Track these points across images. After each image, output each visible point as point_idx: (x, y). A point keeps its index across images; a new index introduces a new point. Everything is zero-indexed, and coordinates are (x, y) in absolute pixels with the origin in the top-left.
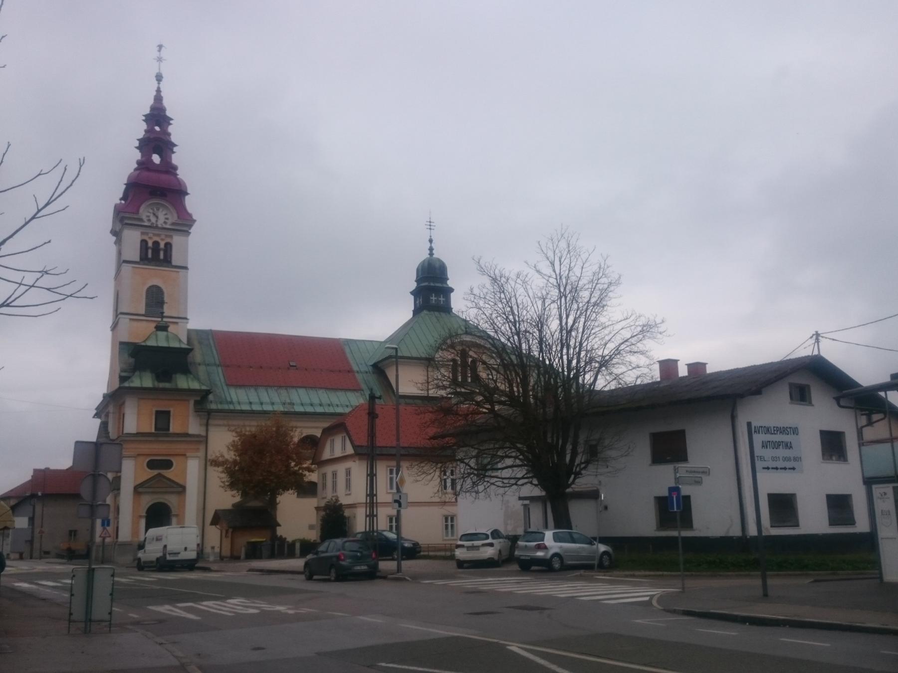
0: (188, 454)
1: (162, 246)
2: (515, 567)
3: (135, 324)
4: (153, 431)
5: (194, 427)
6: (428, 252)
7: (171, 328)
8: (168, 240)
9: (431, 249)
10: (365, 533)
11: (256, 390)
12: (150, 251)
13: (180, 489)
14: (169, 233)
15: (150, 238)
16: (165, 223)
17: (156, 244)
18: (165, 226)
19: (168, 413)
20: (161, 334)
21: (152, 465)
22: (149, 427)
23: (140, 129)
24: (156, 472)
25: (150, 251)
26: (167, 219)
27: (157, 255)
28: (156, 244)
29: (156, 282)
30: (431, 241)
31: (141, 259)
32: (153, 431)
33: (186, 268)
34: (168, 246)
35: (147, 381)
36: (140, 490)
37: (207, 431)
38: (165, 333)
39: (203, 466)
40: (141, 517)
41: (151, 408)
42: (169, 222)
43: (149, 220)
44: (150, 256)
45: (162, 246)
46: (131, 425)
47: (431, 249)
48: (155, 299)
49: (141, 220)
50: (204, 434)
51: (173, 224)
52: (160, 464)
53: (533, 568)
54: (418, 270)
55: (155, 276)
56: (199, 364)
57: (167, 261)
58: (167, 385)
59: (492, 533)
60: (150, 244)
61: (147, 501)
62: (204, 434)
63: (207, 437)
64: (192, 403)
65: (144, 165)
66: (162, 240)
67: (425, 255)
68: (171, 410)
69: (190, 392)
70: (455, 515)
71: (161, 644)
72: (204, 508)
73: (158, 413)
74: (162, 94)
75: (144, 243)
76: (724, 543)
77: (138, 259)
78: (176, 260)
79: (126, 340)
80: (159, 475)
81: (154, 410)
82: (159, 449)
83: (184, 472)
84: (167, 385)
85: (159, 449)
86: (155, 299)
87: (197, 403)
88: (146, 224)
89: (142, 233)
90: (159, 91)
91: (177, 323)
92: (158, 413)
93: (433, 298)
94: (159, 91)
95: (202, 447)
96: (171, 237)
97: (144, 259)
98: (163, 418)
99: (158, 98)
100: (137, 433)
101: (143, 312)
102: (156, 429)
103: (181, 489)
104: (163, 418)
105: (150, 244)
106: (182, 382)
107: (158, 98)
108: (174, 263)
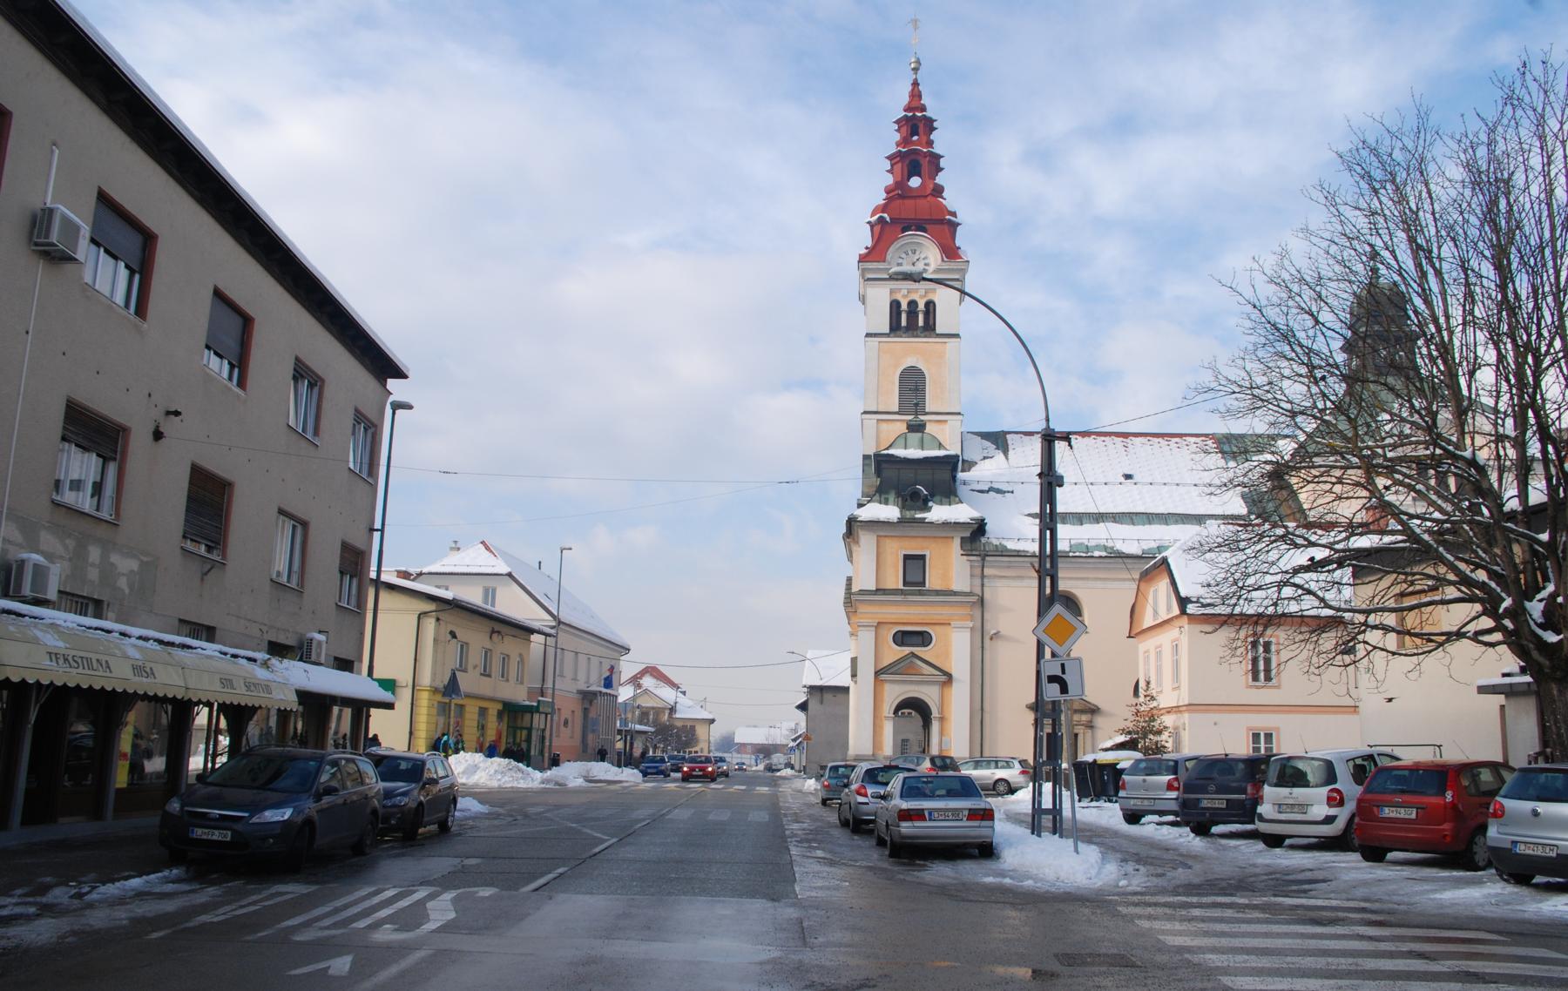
1: (921, 306)
2: (874, 842)
3: (884, 426)
4: (901, 586)
7: (929, 428)
8: (930, 297)
10: (449, 798)
12: (904, 316)
13: (944, 678)
17: (913, 304)
19: (923, 557)
21: (902, 638)
22: (895, 580)
23: (890, 140)
24: (907, 650)
25: (904, 316)
28: (913, 304)
31: (892, 329)
32: (901, 586)
34: (930, 306)
36: (883, 677)
41: (896, 550)
44: (904, 323)
45: (921, 306)
48: (913, 384)
51: (937, 271)
55: (911, 351)
57: (930, 328)
60: (904, 306)
61: (894, 693)
64: (957, 542)
65: (897, 193)
68: (928, 554)
69: (946, 525)
75: (895, 306)
76: (1089, 841)
85: (910, 614)
86: (913, 384)
90: (915, 84)
94: (915, 84)
95: (978, 613)
97: (895, 327)
98: (915, 563)
100: (878, 591)
104: (915, 563)
106: (939, 513)
108: (939, 330)
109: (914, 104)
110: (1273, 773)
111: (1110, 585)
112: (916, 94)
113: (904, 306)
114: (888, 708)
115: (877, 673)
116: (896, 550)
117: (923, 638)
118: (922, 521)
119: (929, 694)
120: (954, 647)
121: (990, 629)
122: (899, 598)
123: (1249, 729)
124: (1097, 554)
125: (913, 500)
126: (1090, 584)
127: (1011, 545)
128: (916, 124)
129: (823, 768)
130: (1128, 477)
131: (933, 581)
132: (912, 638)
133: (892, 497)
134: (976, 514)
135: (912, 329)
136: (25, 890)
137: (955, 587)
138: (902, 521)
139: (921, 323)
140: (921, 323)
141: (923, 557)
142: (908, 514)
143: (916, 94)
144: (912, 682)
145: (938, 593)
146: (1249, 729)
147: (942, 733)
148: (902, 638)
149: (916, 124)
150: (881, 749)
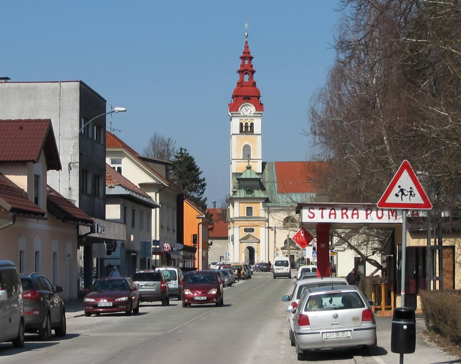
4: (246, 216)
5: (263, 214)
11: (341, 87)
12: (244, 128)
15: (244, 121)
17: (246, 123)
18: (250, 115)
19: (252, 208)
20: (249, 171)
21: (246, 230)
23: (238, 64)
24: (248, 233)
25: (244, 128)
26: (251, 111)
29: (246, 143)
31: (240, 132)
32: (246, 216)
34: (252, 124)
35: (242, 193)
36: (242, 241)
38: (250, 170)
41: (245, 206)
42: (252, 113)
43: (243, 113)
44: (244, 130)
45: (249, 125)
49: (240, 114)
51: (254, 114)
56: (267, 182)
58: (250, 196)
59: (431, 62)
60: (244, 125)
61: (245, 245)
65: (241, 84)
66: (249, 122)
75: (241, 124)
77: (239, 133)
80: (249, 234)
82: (247, 224)
83: (258, 234)
84: (250, 196)
85: (247, 224)
88: (242, 115)
91: (257, 162)
97: (241, 131)
98: (249, 210)
101: (242, 158)
102: (247, 215)
104: (249, 210)
108: (255, 133)
109: (247, 51)
112: (247, 47)
113: (244, 125)
115: (240, 240)
119: (254, 245)
125: (250, 191)
128: (247, 57)
130: (21, 128)
131: (254, 214)
134: (267, 189)
136: (201, 200)
137: (261, 216)
139: (249, 130)
140: (249, 130)
143: (247, 47)
145: (256, 218)
147: (258, 256)
149: (247, 57)
150: (241, 260)
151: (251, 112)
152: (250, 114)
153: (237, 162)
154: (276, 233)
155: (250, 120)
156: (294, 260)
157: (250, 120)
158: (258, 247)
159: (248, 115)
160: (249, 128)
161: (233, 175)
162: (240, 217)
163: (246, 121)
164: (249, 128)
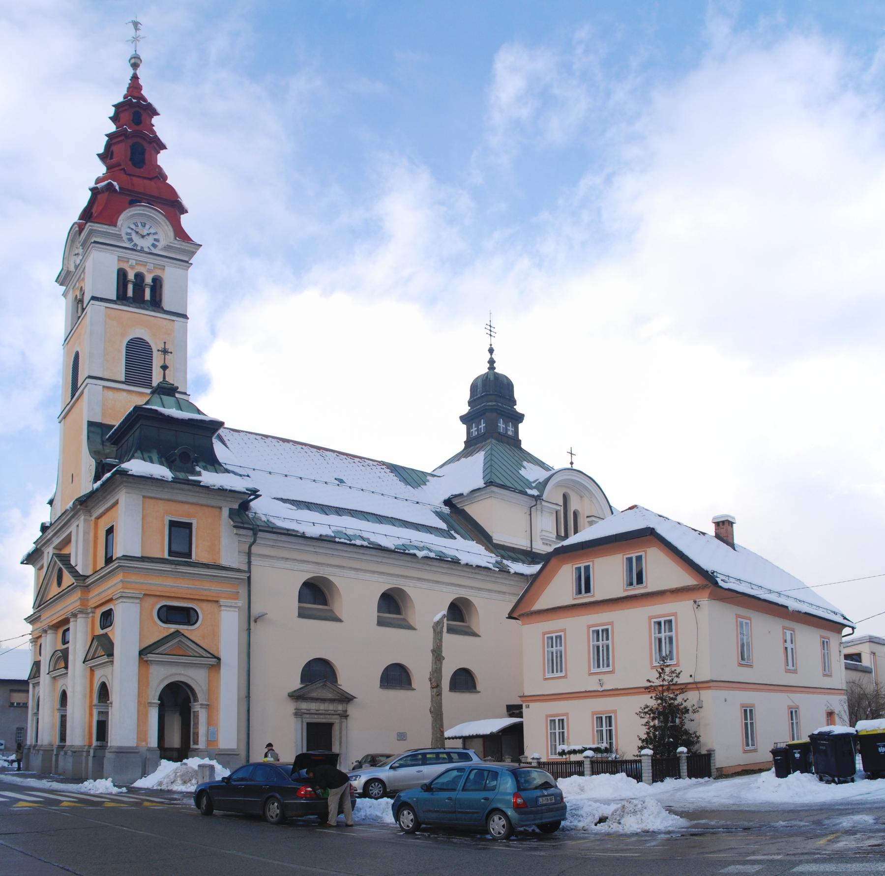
0: (222, 601)
1: (148, 280)
3: (110, 394)
4: (166, 556)
6: (488, 365)
8: (158, 273)
9: (492, 362)
12: (130, 288)
13: (213, 661)
14: (161, 261)
15: (132, 267)
16: (154, 246)
17: (139, 277)
19: (189, 526)
21: (169, 614)
24: (173, 628)
25: (130, 288)
27: (140, 293)
28: (139, 277)
30: (491, 351)
32: (166, 556)
33: (185, 316)
34: (157, 284)
36: (151, 657)
37: (249, 563)
39: (246, 626)
40: (151, 704)
41: (166, 512)
42: (162, 243)
43: (131, 240)
44: (130, 293)
45: (148, 280)
46: (127, 543)
47: (492, 362)
49: (118, 237)
50: (244, 567)
51: (168, 248)
52: (178, 615)
53: (867, 819)
54: (474, 388)
55: (140, 324)
57: (156, 303)
60: (131, 276)
61: (162, 675)
62: (244, 567)
63: (249, 571)
64: (225, 512)
66: (150, 271)
67: (484, 369)
68: (194, 522)
69: (222, 492)
70: (753, 706)
71: (602, 820)
72: (248, 697)
73: (173, 525)
74: (141, 82)
75: (122, 275)
77: (115, 298)
78: (168, 302)
79: (98, 419)
80: (177, 631)
81: (167, 519)
83: (215, 633)
85: (177, 586)
86: (138, 356)
87: (232, 514)
89: (120, 259)
90: (135, 78)
92: (173, 525)
93: (501, 425)
94: (135, 78)
95: (243, 591)
96: (163, 268)
97: (122, 297)
98: (180, 531)
99: (135, 85)
102: (171, 553)
103: (215, 662)
104: (180, 531)
105: (131, 276)
107: (135, 85)
110: (587, 766)
111: (361, 575)
114: (154, 696)
115: (141, 653)
116: (166, 512)
117: (186, 616)
118: (197, 484)
119: (196, 678)
120: (224, 628)
121: (256, 610)
122: (168, 567)
123: (593, 713)
124: (359, 542)
126: (345, 572)
127: (280, 523)
129: (659, 623)
132: (178, 615)
133: (155, 457)
135: (138, 300)
137: (224, 562)
138: (175, 480)
141: (189, 526)
142: (181, 475)
144: (178, 664)
146: (593, 713)
147: (210, 722)
148: (169, 614)
151: (156, 243)
152: (152, 248)
153: (104, 387)
154: (430, 646)
155: (151, 266)
156: (330, 747)
157: (151, 266)
158: (213, 689)
159: (146, 250)
160: (148, 292)
161: (92, 429)
162: (143, 559)
163: (140, 269)
164: (148, 292)
